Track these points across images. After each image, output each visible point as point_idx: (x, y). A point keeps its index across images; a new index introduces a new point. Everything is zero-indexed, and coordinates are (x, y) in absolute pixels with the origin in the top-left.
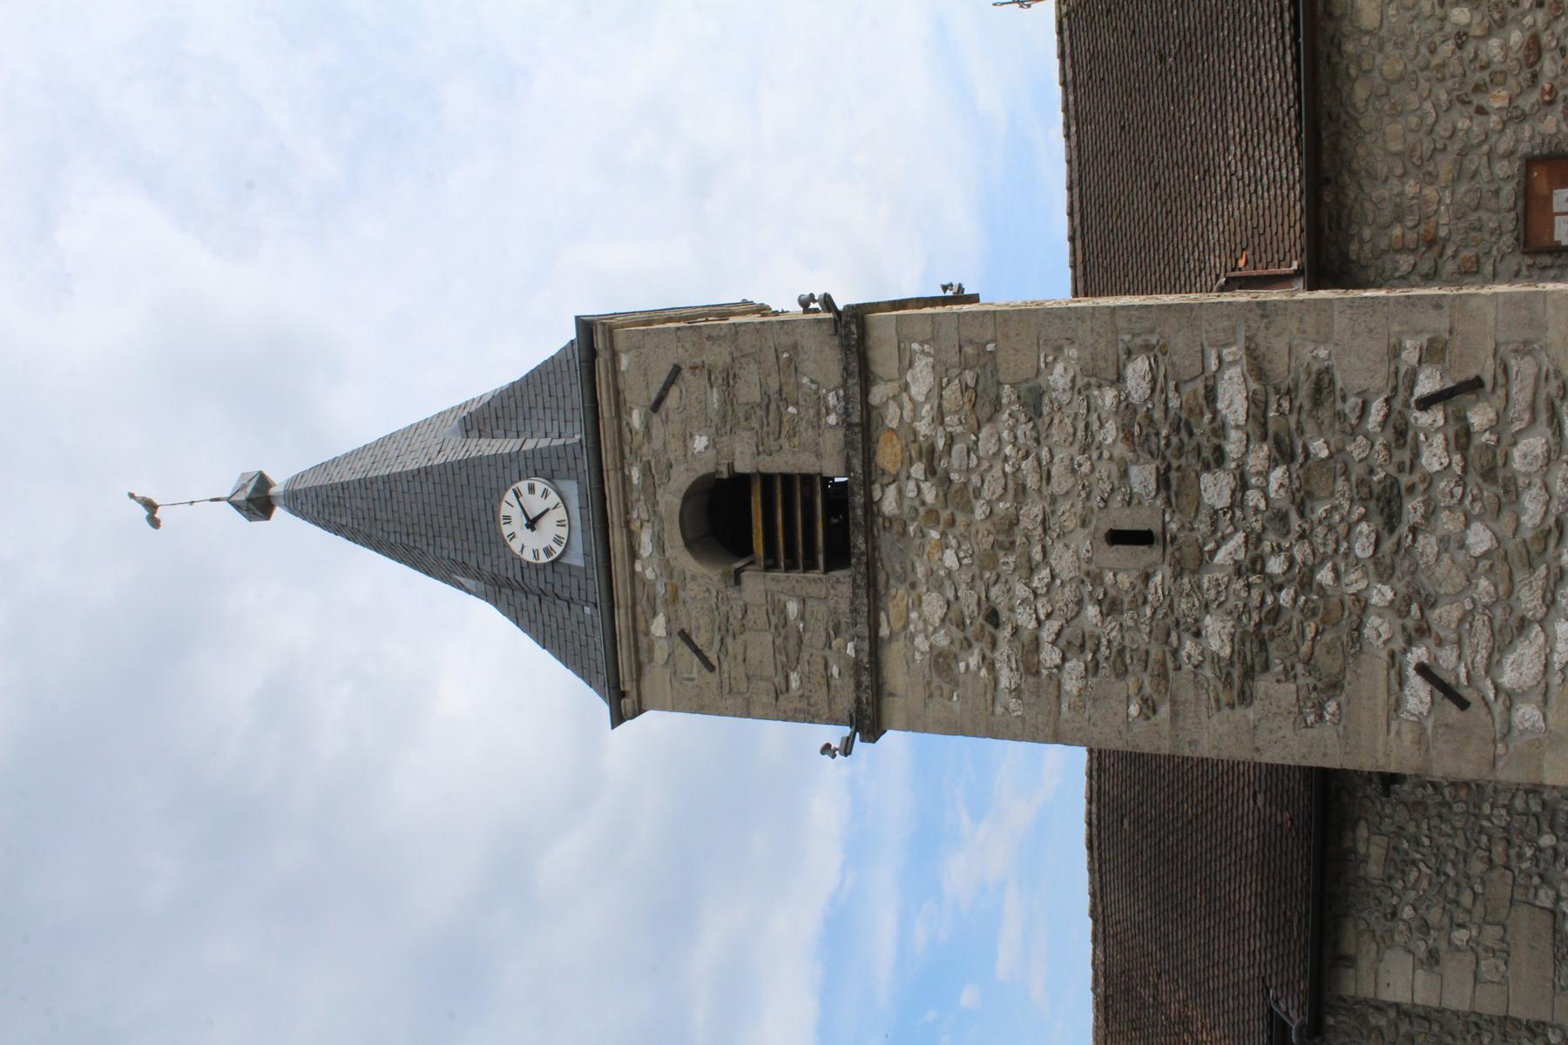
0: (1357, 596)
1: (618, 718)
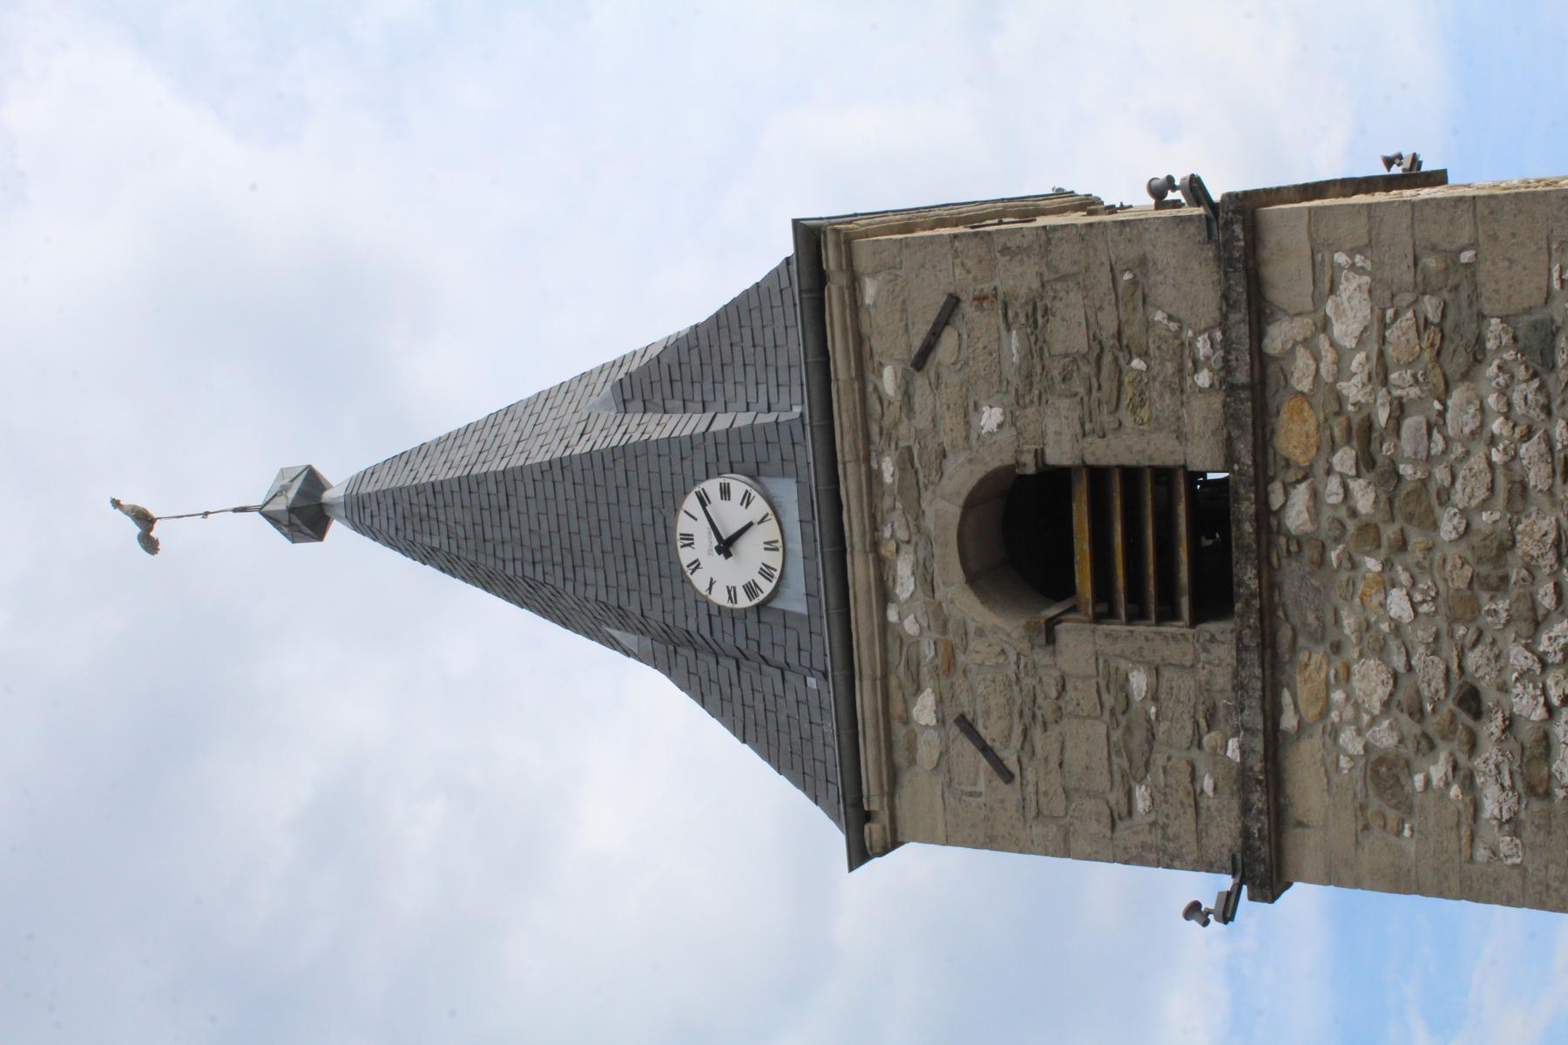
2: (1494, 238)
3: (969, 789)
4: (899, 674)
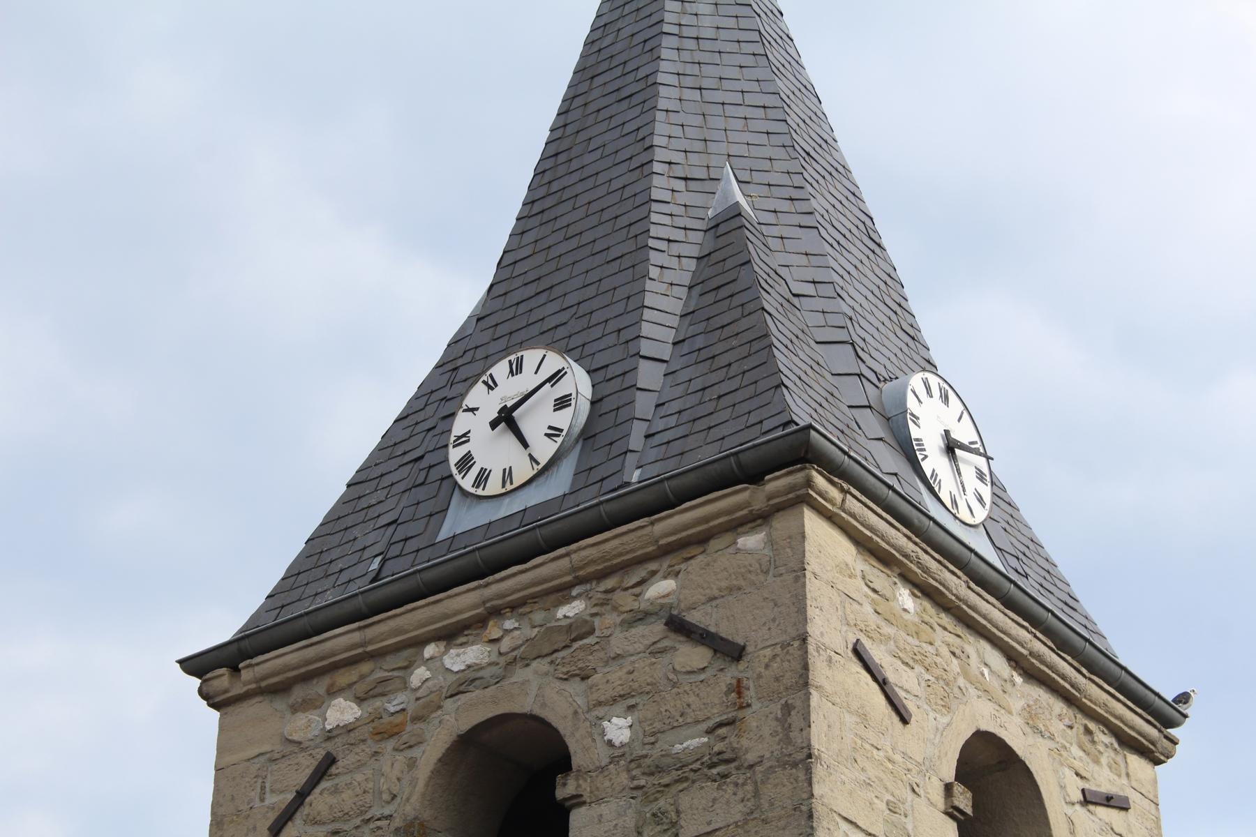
3: (268, 785)
4: (375, 672)
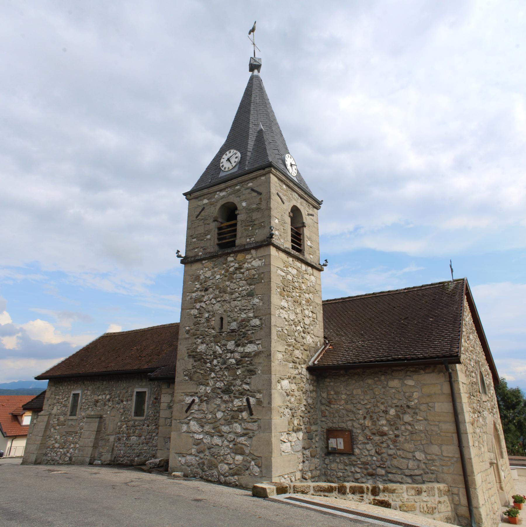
0: (208, 384)
1: (185, 194)
2: (265, 285)
